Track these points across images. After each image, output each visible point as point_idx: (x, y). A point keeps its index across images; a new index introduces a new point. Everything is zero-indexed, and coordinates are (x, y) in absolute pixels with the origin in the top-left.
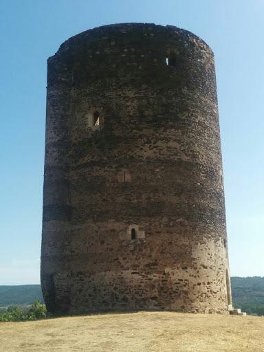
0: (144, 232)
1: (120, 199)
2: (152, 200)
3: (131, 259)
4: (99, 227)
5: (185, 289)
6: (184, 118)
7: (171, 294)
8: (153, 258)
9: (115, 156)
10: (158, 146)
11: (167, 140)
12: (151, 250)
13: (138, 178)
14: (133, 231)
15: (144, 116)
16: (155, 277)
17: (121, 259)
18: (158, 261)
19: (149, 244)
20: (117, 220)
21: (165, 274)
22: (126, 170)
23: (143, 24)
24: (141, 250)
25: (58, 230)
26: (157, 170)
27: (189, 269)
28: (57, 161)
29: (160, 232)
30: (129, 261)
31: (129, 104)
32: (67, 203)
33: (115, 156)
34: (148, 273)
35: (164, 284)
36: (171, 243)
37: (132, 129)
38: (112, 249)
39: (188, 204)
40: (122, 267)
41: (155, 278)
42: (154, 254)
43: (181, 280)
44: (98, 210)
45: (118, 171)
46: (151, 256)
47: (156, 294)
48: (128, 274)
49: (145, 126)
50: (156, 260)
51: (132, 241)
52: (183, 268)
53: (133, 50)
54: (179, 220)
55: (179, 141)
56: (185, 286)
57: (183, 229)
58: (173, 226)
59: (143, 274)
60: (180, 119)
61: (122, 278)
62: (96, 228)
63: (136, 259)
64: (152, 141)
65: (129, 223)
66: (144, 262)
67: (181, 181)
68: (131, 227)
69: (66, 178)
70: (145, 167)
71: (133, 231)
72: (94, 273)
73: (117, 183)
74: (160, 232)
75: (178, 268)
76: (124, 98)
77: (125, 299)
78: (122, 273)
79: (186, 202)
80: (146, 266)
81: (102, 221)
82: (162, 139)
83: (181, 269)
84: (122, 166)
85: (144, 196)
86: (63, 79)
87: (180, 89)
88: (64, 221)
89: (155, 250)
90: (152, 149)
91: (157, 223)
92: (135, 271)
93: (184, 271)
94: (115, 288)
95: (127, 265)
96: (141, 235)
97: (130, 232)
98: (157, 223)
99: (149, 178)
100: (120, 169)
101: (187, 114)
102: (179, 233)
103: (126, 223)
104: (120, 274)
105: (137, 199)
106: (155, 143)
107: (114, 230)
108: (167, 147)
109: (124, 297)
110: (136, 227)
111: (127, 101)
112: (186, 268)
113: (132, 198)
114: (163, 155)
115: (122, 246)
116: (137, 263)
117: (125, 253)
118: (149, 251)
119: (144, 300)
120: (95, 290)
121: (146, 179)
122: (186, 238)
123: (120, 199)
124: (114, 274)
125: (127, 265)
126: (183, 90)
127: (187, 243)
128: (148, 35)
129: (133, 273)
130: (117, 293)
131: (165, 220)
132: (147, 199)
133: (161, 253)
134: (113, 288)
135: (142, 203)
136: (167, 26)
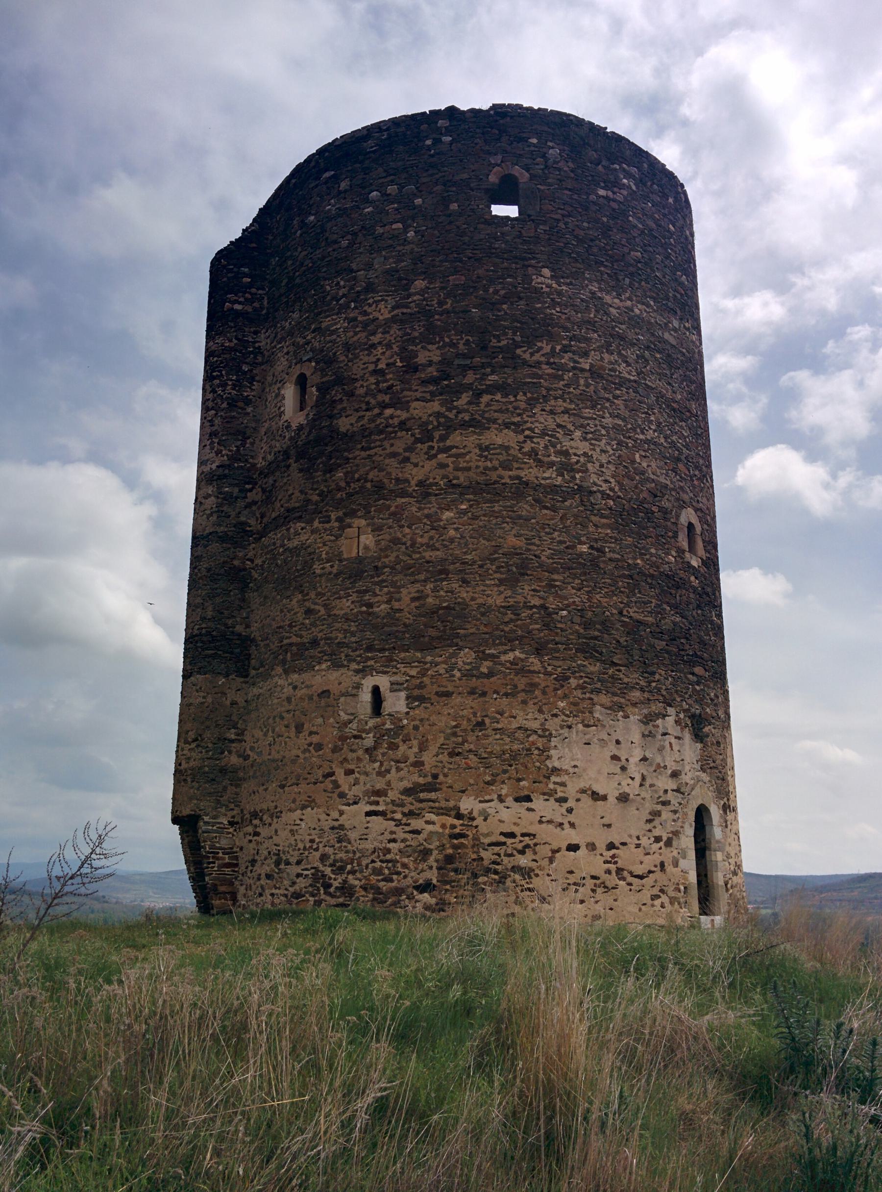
0: (403, 694)
1: (345, 606)
2: (430, 600)
3: (366, 774)
4: (295, 688)
5: (523, 861)
6: (537, 357)
7: (475, 876)
8: (427, 767)
9: (339, 489)
10: (450, 448)
11: (476, 424)
12: (423, 748)
13: (396, 541)
14: (376, 691)
15: (416, 369)
16: (432, 825)
17: (340, 773)
18: (441, 777)
19: (416, 728)
20: (337, 665)
21: (459, 816)
22: (363, 522)
23: (423, 114)
24: (393, 747)
25: (209, 700)
26: (447, 515)
27: (538, 803)
28: (214, 518)
29: (448, 694)
30: (362, 778)
31: (375, 339)
32: (239, 628)
33: (339, 489)
34: (411, 814)
35: (455, 847)
36: (481, 725)
37: (384, 406)
38: (319, 747)
39: (543, 607)
40: (342, 795)
41: (430, 828)
42: (427, 758)
43: (512, 835)
44: (294, 639)
45: (342, 528)
46: (422, 764)
47: (433, 876)
48: (354, 816)
49: (418, 395)
50: (435, 776)
51: (371, 723)
52: (517, 800)
53: (392, 189)
54: (510, 656)
55: (518, 428)
56: (522, 852)
57: (522, 683)
58: (490, 674)
59: (398, 816)
60: (525, 362)
61: (342, 827)
62: (288, 690)
63: (380, 774)
64: (437, 435)
65: (363, 672)
66: (401, 780)
67: (520, 543)
68: (369, 683)
69: (236, 563)
70: (414, 509)
71: (376, 691)
72: (276, 814)
73: (340, 561)
74: (448, 694)
75: (501, 799)
76: (365, 325)
77: (346, 890)
78: (341, 813)
79: (536, 602)
80: (407, 792)
81: (301, 671)
82: (464, 425)
83: (510, 801)
84: (353, 514)
85: (406, 594)
86: (238, 307)
87: (527, 279)
88: (227, 676)
89: (433, 749)
90: (435, 456)
91: (442, 669)
92: (373, 808)
93: (520, 808)
94: (324, 858)
95: (357, 790)
96: (396, 703)
97: (366, 697)
98: (442, 669)
99: (425, 540)
100: (348, 520)
101: (547, 349)
102: (506, 695)
103: (357, 671)
104: (335, 814)
105: (388, 602)
106: (443, 438)
107: (325, 693)
108: (480, 447)
109: (345, 881)
110: (383, 682)
111: (374, 333)
112: (528, 799)
113: (374, 600)
114: (468, 469)
115: (343, 738)
116: (380, 785)
117: (351, 755)
118: (416, 750)
119: (398, 891)
120: (277, 863)
121: (413, 545)
122: (531, 708)
123: (345, 606)
124: (323, 817)
125: (357, 790)
126: (537, 280)
127: (535, 725)
128: (437, 141)
129: (368, 814)
130: (328, 871)
131: (466, 656)
132: (413, 599)
133: (452, 754)
134: (317, 855)
135: (400, 610)
136: (494, 107)
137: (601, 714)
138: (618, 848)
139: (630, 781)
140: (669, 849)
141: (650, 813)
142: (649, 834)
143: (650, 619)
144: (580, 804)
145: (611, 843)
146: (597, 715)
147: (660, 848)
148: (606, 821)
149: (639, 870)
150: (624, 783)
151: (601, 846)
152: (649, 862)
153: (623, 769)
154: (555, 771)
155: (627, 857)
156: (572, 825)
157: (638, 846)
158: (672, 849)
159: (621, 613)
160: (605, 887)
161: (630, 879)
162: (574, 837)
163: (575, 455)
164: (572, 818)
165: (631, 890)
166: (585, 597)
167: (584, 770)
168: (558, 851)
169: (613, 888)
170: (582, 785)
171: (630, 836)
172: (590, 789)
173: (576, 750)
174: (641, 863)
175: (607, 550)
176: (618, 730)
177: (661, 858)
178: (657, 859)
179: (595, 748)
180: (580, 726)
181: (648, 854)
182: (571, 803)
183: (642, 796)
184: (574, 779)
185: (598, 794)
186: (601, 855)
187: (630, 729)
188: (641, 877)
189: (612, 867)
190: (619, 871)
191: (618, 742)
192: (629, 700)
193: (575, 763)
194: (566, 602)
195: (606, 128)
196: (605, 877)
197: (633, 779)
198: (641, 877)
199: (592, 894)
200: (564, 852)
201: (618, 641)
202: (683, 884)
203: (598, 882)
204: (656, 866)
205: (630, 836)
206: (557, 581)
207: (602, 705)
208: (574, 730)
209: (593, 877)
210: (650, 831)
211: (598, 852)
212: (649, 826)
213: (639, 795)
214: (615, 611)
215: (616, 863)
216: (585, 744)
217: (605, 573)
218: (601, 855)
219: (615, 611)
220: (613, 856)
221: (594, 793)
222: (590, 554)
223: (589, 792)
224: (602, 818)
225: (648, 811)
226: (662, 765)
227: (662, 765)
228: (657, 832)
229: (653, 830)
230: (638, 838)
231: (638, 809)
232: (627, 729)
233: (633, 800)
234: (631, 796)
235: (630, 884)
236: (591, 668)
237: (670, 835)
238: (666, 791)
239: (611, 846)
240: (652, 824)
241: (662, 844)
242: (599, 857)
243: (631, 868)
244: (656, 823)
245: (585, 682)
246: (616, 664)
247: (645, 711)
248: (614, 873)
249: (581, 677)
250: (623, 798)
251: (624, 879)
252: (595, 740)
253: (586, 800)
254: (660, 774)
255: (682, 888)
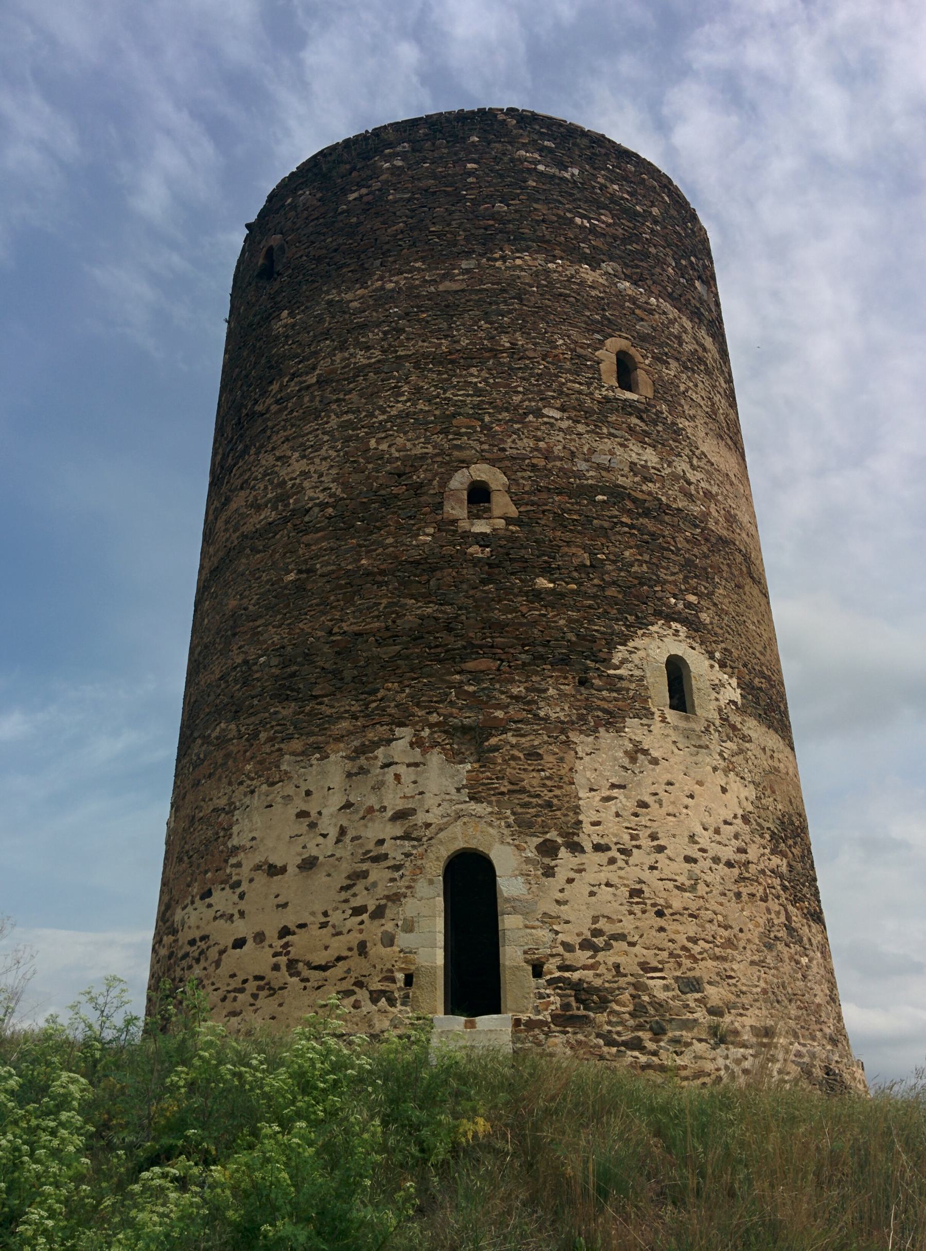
137: (289, 765)
138: (294, 933)
139: (320, 840)
140: (377, 922)
141: (348, 877)
142: (345, 906)
143: (377, 624)
144: (254, 885)
145: (285, 927)
146: (284, 767)
147: (362, 923)
148: (281, 900)
149: (320, 958)
150: (311, 845)
151: (271, 933)
152: (338, 945)
153: (313, 826)
154: (235, 850)
155: (310, 945)
156: (242, 914)
157: (323, 925)
158: (383, 921)
159: (330, 633)
160: (270, 989)
161: (306, 973)
162: (241, 928)
163: (291, 479)
164: (243, 905)
165: (305, 988)
166: (285, 632)
167: (262, 841)
168: (224, 951)
169: (281, 989)
170: (258, 858)
171: (313, 914)
172: (266, 862)
173: (257, 818)
174: (326, 948)
175: (318, 566)
176: (309, 778)
177: (361, 937)
178: (354, 938)
179: (278, 808)
180: (264, 787)
181: (339, 933)
182: (244, 887)
183: (338, 855)
184: (249, 855)
185: (276, 866)
186: (271, 946)
187: (333, 769)
188: (323, 968)
189: (283, 960)
190: (292, 964)
191: (308, 793)
192: (330, 736)
193: (254, 834)
194: (265, 646)
195: (367, 131)
196: (271, 975)
197: (324, 836)
198: (323, 968)
199: (252, 1001)
200: (231, 951)
201: (323, 668)
202: (401, 970)
203: (262, 983)
204: (350, 949)
205: (313, 914)
206: (259, 626)
207: (293, 754)
208: (256, 794)
209: (258, 978)
210: (346, 901)
211: (266, 943)
212: (344, 895)
213: (333, 855)
214: (320, 633)
215: (288, 953)
216: (267, 807)
217: (313, 593)
218: (271, 946)
219: (320, 633)
220: (286, 945)
221: (271, 866)
222: (299, 579)
223: (265, 867)
224: (277, 896)
225: (345, 875)
226: (377, 807)
227: (377, 807)
228: (356, 902)
229: (352, 899)
230: (325, 914)
231: (329, 875)
232: (323, 773)
233: (322, 864)
234: (321, 858)
235: (307, 980)
236: (285, 712)
237: (383, 902)
238: (381, 842)
239: (285, 932)
240: (350, 892)
241: (365, 917)
242: (267, 949)
243: (309, 957)
244: (359, 887)
245: (275, 732)
246: (316, 697)
247: (356, 743)
248: (284, 968)
249: (272, 727)
250: (309, 864)
251: (298, 974)
252: (279, 799)
253: (261, 878)
254: (371, 820)
255: (400, 976)
